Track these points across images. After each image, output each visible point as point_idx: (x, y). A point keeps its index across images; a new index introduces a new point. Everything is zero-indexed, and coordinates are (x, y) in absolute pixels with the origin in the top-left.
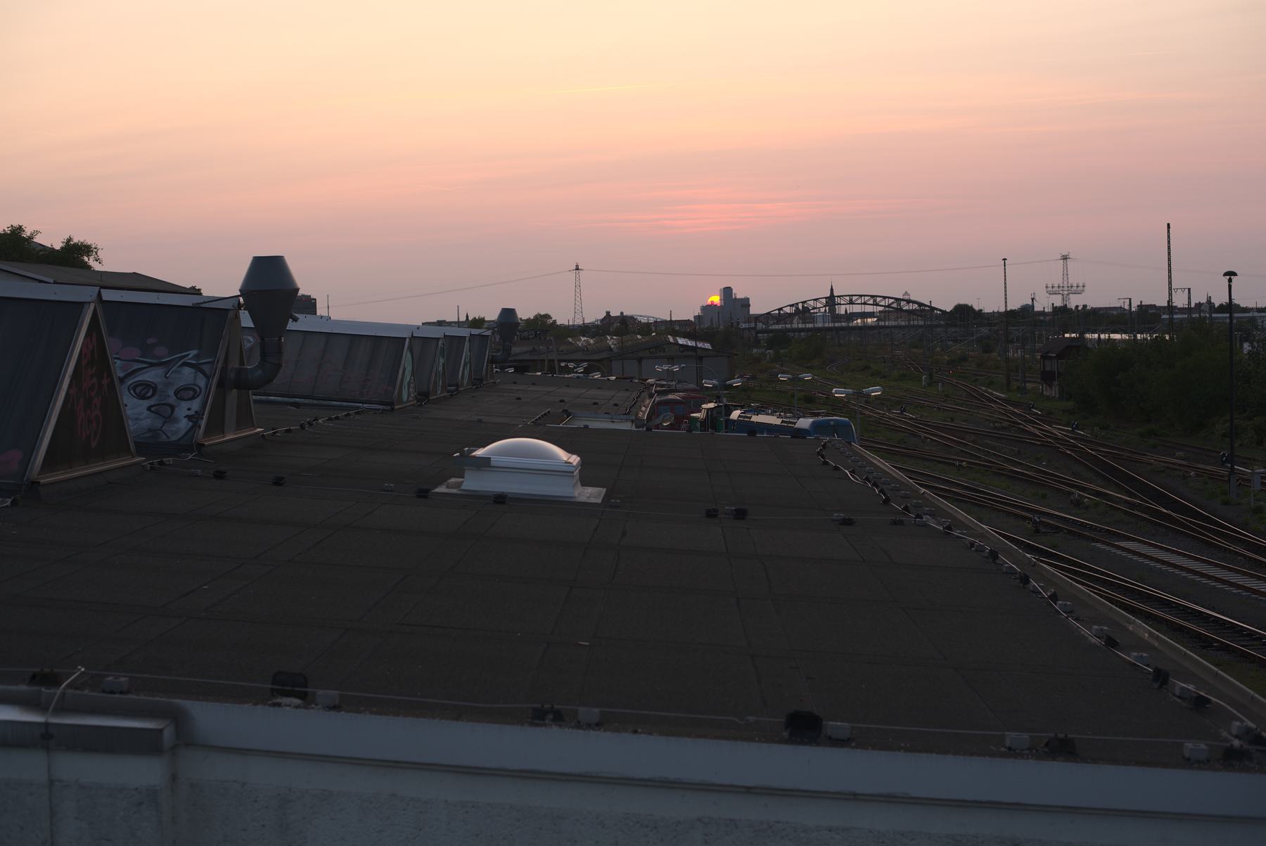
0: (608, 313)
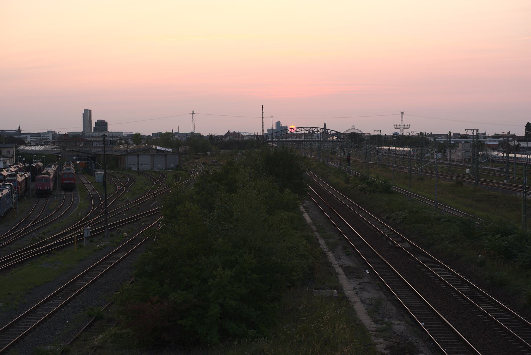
0: (229, 131)
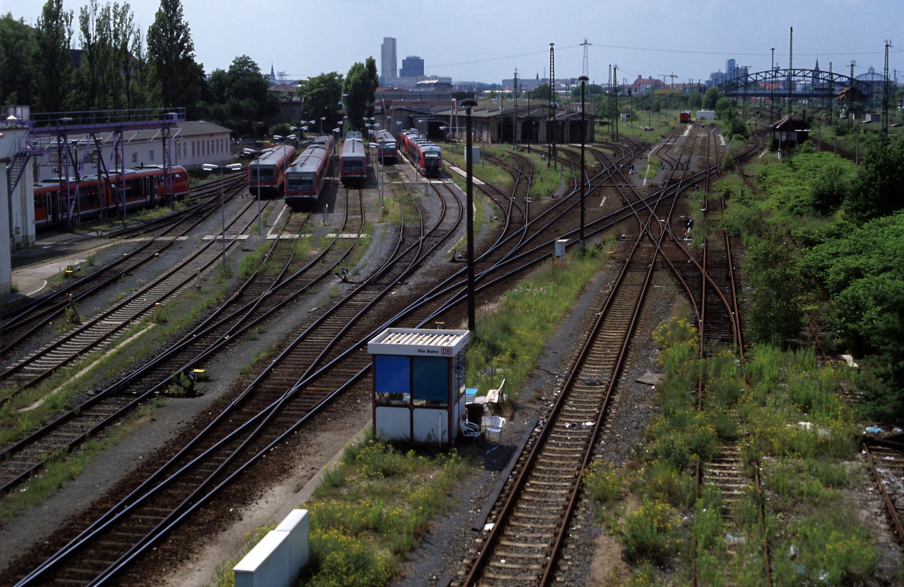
0: (640, 76)
